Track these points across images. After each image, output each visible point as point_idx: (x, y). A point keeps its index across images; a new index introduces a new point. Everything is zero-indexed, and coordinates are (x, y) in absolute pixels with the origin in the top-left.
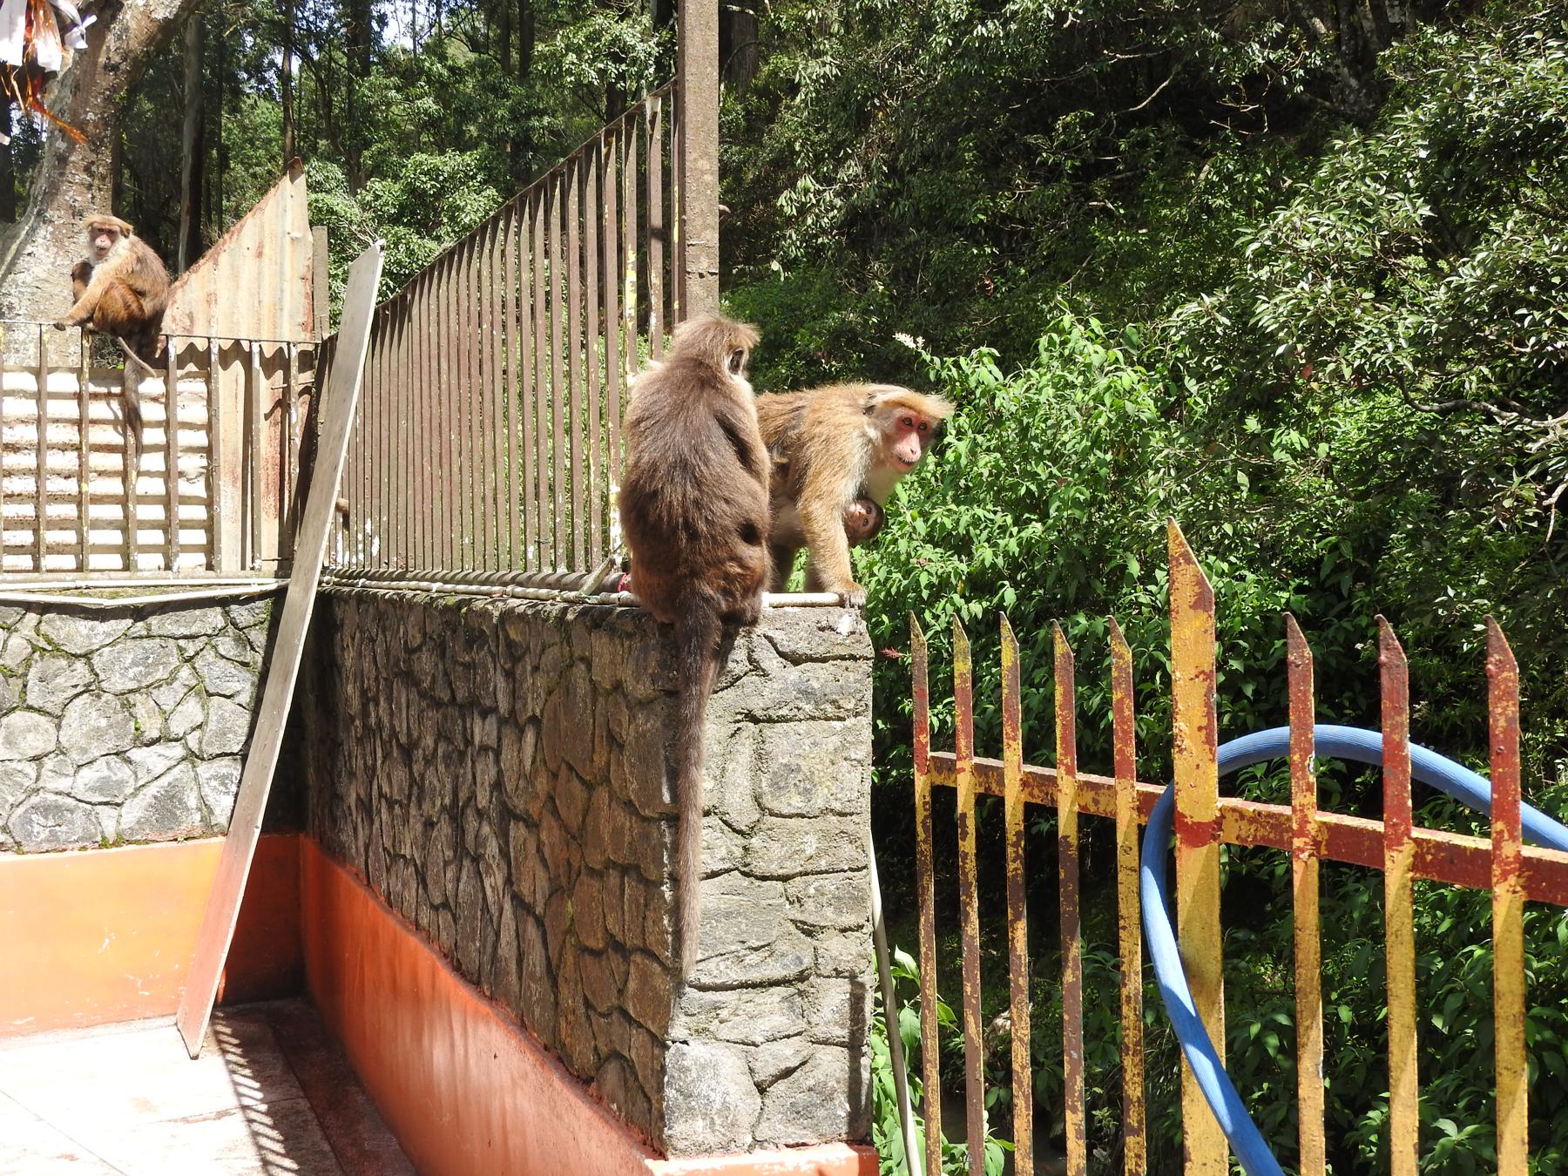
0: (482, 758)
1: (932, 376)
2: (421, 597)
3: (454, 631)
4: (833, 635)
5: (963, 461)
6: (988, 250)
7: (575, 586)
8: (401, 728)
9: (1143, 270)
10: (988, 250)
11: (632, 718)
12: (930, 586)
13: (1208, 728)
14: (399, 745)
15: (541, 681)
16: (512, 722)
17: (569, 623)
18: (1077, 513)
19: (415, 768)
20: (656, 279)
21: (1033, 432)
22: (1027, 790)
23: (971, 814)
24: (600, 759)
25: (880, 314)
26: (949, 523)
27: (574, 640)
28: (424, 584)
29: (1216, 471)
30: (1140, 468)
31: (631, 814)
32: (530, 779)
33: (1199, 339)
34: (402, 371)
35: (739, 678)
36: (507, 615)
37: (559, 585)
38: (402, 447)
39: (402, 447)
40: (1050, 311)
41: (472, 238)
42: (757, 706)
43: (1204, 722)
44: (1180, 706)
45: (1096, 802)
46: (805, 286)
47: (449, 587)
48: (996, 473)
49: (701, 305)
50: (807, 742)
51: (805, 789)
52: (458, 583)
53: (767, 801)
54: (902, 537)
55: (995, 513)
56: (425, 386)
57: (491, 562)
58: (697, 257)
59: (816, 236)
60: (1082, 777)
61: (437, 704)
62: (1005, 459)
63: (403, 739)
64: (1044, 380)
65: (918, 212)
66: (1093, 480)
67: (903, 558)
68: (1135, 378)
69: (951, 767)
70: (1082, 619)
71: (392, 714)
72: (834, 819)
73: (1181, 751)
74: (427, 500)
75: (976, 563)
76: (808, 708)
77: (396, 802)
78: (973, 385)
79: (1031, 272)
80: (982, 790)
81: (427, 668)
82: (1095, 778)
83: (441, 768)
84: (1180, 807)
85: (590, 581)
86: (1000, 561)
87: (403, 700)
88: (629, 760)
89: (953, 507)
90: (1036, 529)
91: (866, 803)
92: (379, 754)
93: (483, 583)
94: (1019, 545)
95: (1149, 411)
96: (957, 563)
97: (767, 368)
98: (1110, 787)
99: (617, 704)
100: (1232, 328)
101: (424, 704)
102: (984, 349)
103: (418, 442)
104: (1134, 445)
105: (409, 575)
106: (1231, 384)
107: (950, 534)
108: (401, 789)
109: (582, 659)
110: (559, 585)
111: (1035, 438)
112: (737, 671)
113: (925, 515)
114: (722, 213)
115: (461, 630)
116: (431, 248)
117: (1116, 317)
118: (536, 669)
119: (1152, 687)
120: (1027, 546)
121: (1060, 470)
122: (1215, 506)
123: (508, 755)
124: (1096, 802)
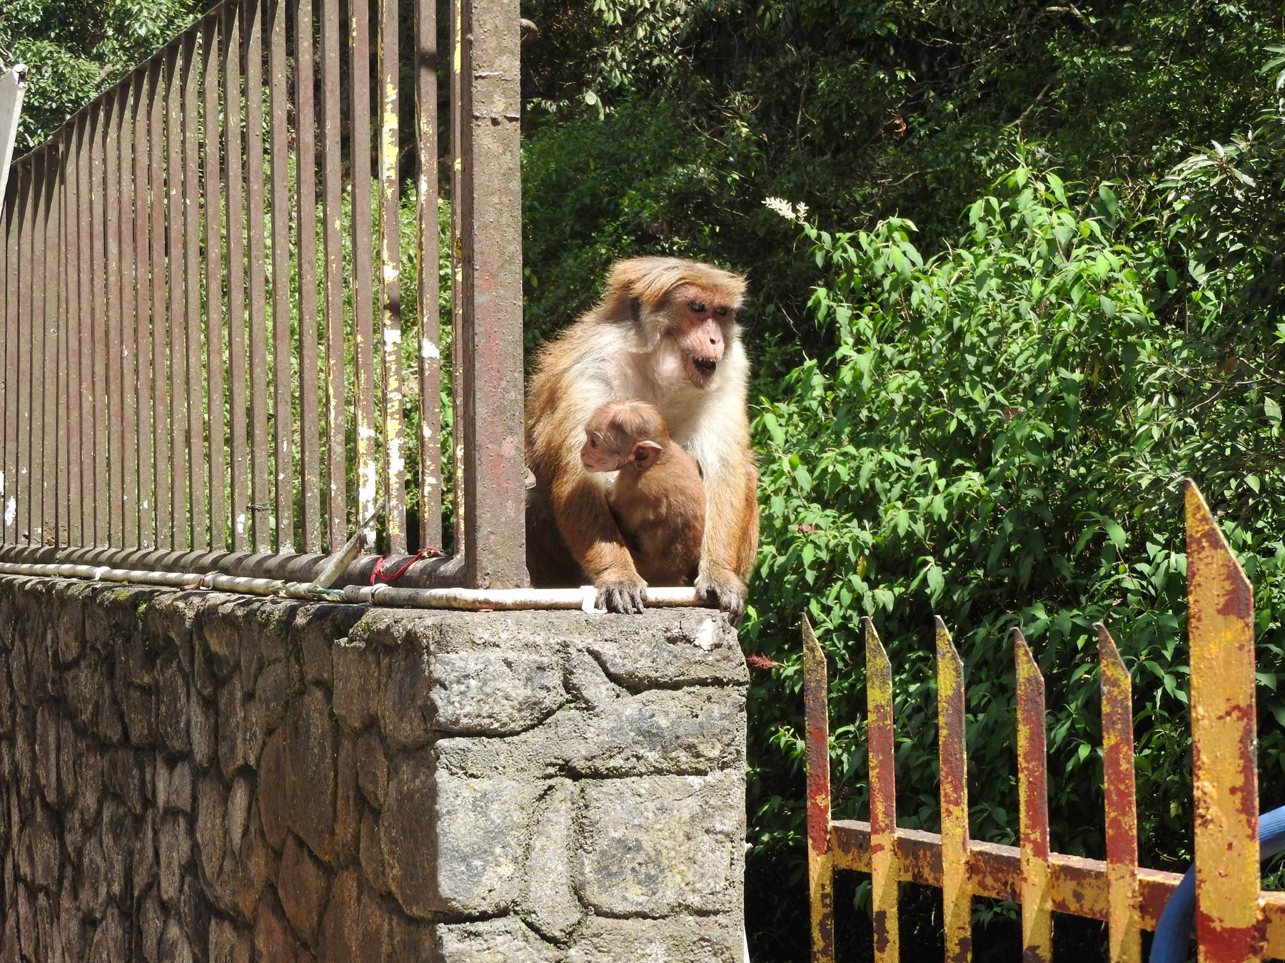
0: (168, 827)
1: (819, 260)
2: (79, 588)
3: (127, 639)
4: (688, 649)
5: (866, 383)
6: (901, 75)
7: (307, 574)
8: (49, 779)
9: (1126, 104)
10: (901, 75)
11: (393, 772)
12: (817, 564)
13: (1246, 788)
14: (46, 805)
15: (256, 715)
16: (212, 773)
17: (298, 630)
18: (1033, 459)
19: (69, 838)
20: (427, 126)
21: (970, 339)
22: (976, 878)
23: (893, 912)
24: (344, 832)
25: (742, 167)
26: (844, 473)
27: (307, 657)
28: (82, 568)
29: (1236, 397)
30: (1126, 395)
31: (391, 912)
32: (240, 860)
33: (1212, 203)
34: (51, 256)
35: (550, 713)
36: (207, 617)
37: (285, 573)
38: (50, 366)
39: (50, 366)
40: (991, 163)
41: (154, 64)
42: (577, 753)
43: (1239, 781)
44: (1204, 758)
45: (1078, 896)
46: (634, 127)
47: (119, 573)
48: (914, 398)
49: (494, 166)
50: (651, 806)
51: (648, 876)
52: (134, 567)
53: (594, 895)
54: (776, 492)
55: (912, 457)
56: (85, 277)
57: (183, 537)
58: (489, 96)
59: (650, 55)
60: (1057, 859)
61: (102, 746)
62: (926, 380)
63: (51, 797)
64: (984, 264)
65: (797, 20)
66: (1056, 410)
67: (778, 523)
68: (1116, 261)
69: (862, 843)
70: (1042, 615)
71: (34, 759)
72: (691, 919)
73: (1205, 823)
74: (88, 445)
75: (885, 531)
76: (653, 756)
77: (41, 888)
78: (880, 272)
79: (963, 108)
80: (908, 877)
81: (87, 692)
82: (1076, 861)
83: (108, 840)
84: (1205, 906)
85: (329, 567)
86: (920, 528)
87: (52, 739)
88: (387, 833)
89: (851, 449)
90: (972, 481)
91: (737, 896)
92: (15, 818)
93: (170, 568)
94: (948, 505)
95: (1131, 303)
96: (857, 531)
97: (581, 247)
98: (1099, 875)
99: (370, 750)
100: (1258, 191)
101: (82, 745)
102: (895, 221)
103: (73, 360)
104: (1115, 360)
105: (60, 555)
106: (1255, 269)
107: (846, 488)
108: (47, 870)
109: (318, 683)
110: (285, 573)
111: (972, 349)
112: (547, 703)
113: (809, 461)
114: (525, 30)
115: (137, 638)
116: (92, 74)
117: (1083, 174)
118: (249, 696)
119: (1163, 720)
120: (961, 509)
121: (1006, 395)
122: (1234, 449)
123: (207, 822)
124: (1078, 896)
